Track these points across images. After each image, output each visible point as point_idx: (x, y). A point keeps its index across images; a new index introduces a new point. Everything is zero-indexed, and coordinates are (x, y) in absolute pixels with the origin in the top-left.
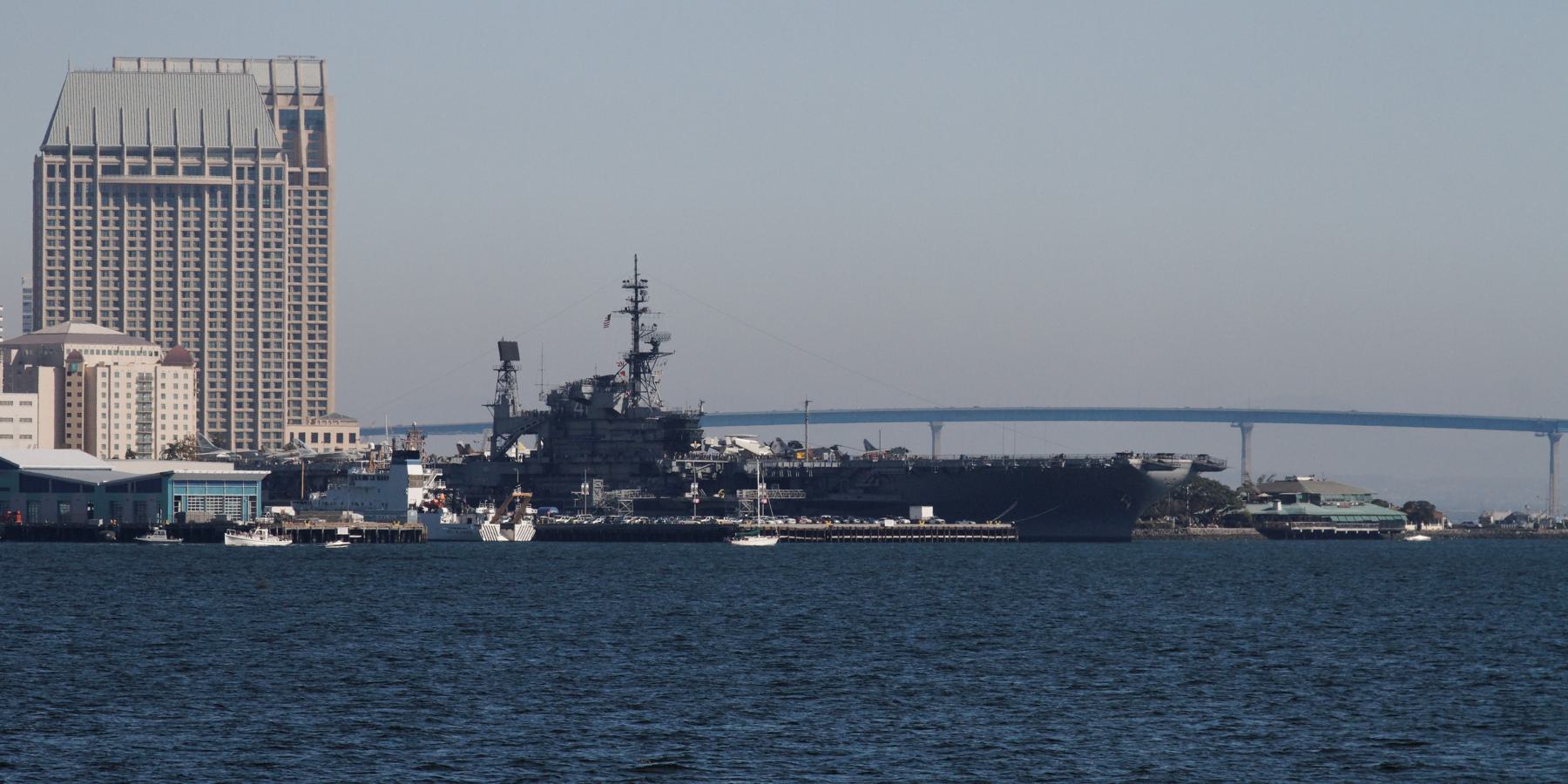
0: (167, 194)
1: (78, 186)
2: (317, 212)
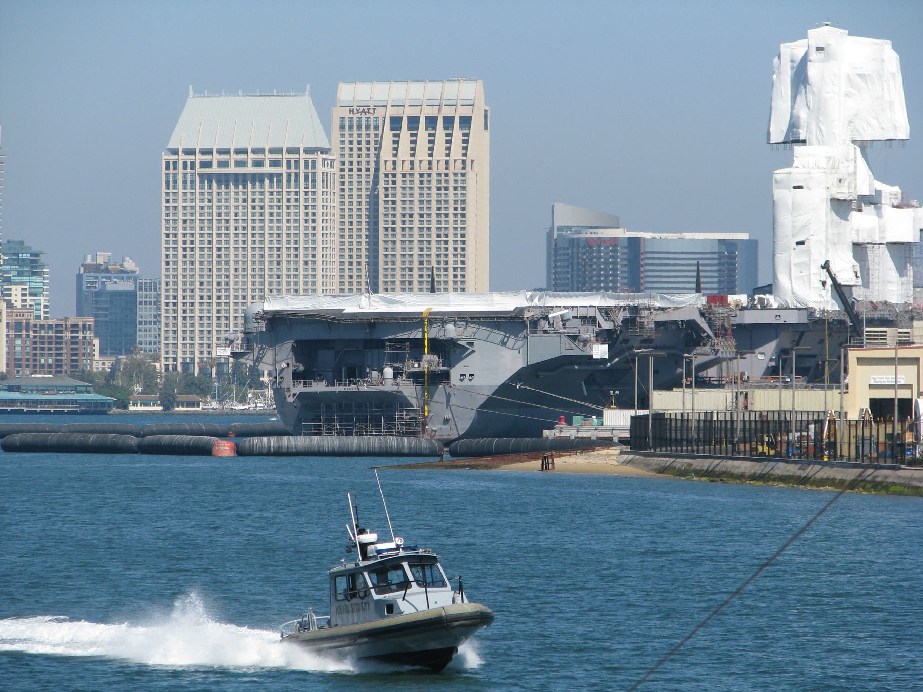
0: (257, 179)
1: (185, 175)
2: (442, 188)
